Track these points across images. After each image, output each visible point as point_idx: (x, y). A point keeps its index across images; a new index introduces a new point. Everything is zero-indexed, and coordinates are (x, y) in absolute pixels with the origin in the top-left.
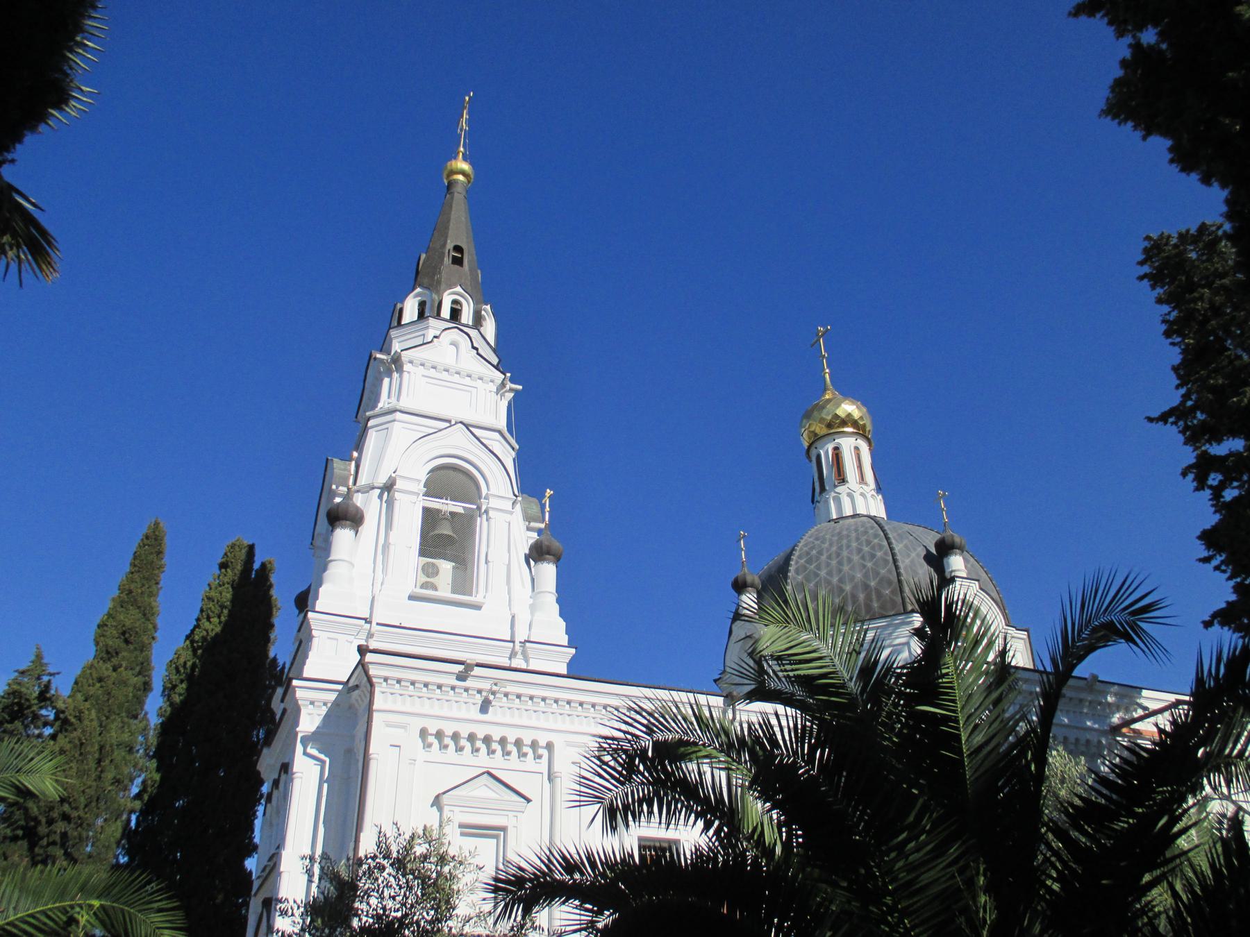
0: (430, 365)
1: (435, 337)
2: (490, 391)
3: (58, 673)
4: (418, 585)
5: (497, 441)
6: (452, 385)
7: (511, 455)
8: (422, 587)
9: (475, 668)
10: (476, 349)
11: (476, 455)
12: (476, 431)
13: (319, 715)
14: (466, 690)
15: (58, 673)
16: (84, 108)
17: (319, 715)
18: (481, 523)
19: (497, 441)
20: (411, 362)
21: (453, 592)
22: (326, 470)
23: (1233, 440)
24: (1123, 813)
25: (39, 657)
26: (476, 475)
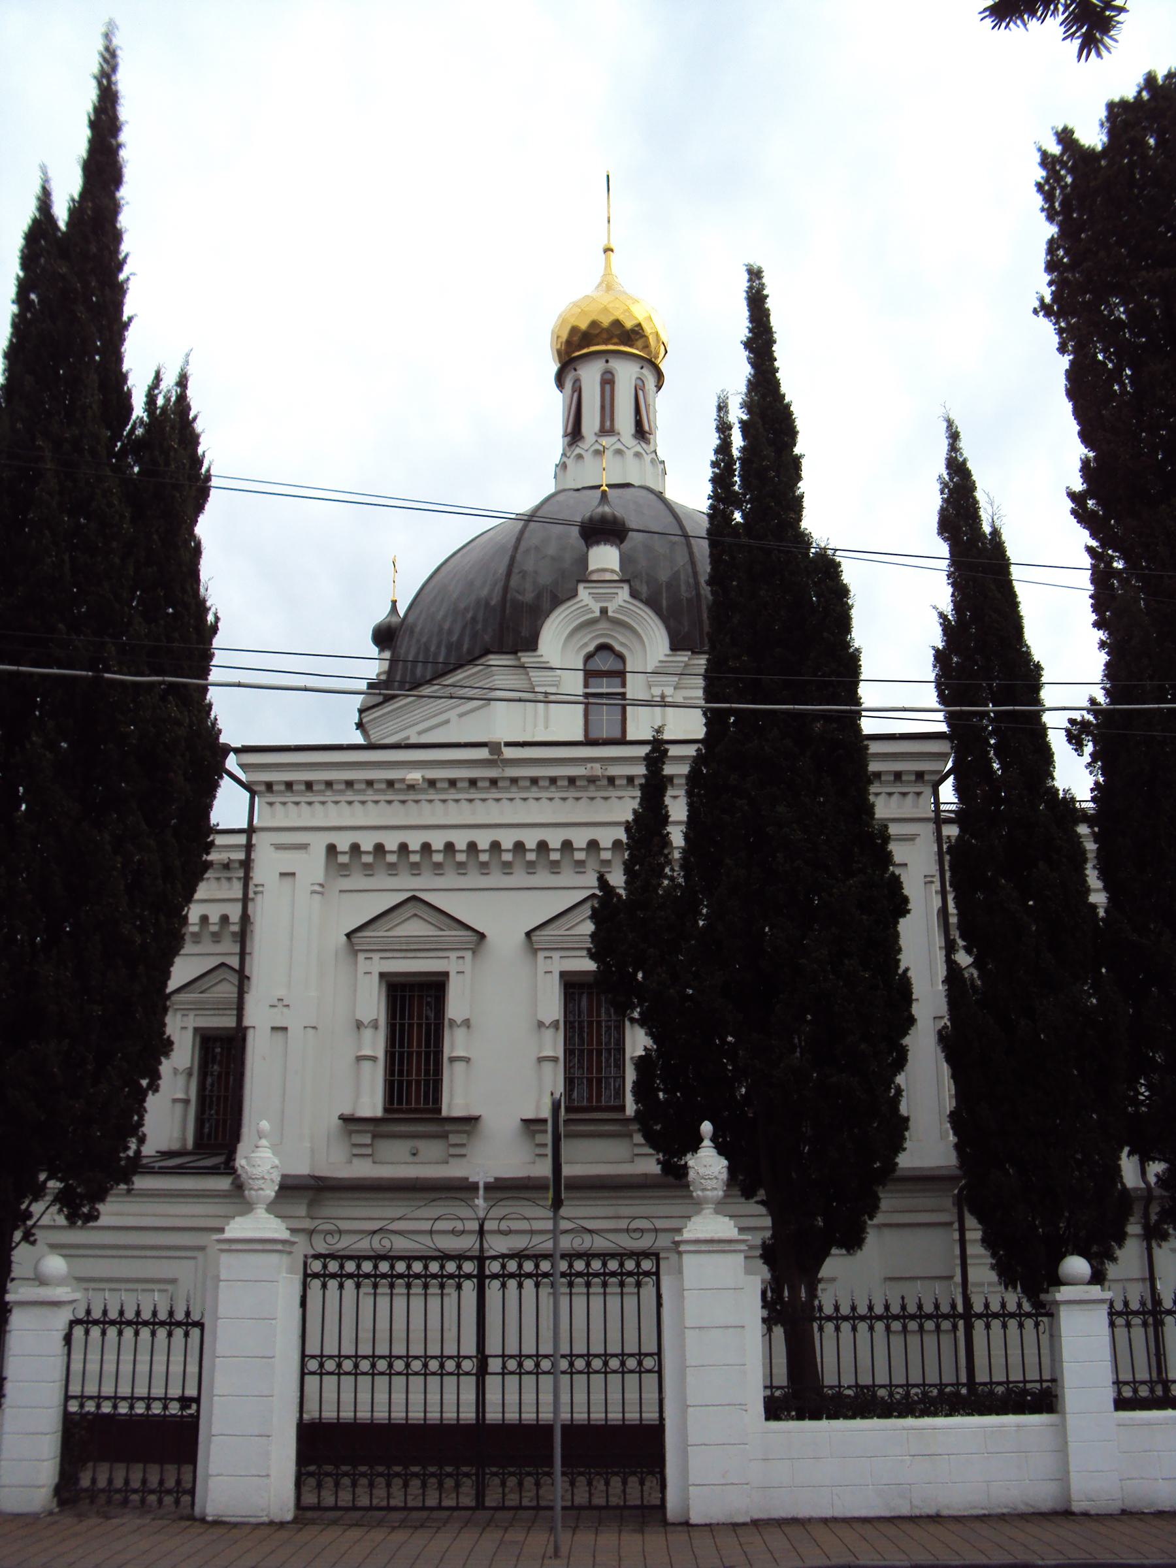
22: (609, 234)
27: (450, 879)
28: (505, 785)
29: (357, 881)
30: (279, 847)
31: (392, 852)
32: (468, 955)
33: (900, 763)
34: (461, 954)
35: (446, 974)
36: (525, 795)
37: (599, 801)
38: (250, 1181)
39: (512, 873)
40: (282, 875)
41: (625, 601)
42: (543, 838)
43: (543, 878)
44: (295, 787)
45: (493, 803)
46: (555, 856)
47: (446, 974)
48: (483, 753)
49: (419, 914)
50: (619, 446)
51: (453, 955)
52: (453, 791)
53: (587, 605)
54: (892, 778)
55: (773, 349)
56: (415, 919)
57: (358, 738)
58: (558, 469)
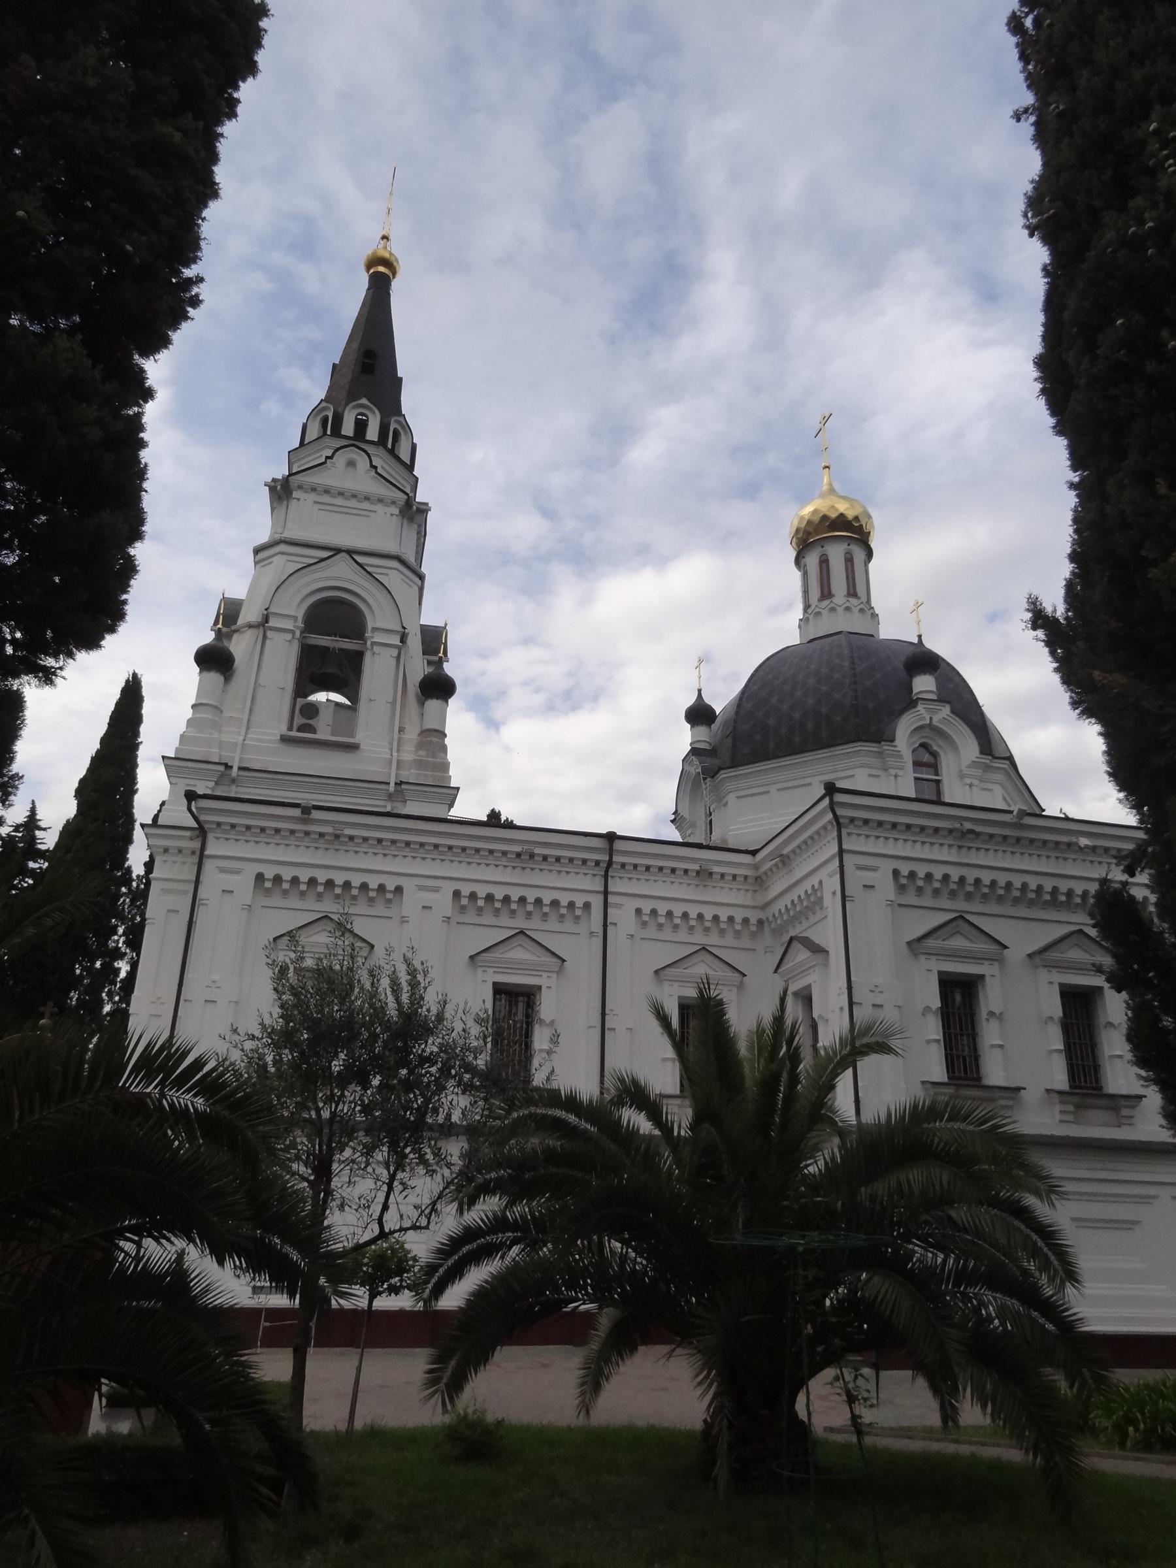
0: (337, 492)
1: (327, 458)
2: (392, 515)
3: (49, 828)
4: (295, 727)
5: (394, 569)
6: (346, 510)
7: (415, 583)
8: (299, 730)
9: (313, 811)
10: (375, 468)
11: (360, 586)
12: (356, 557)
13: (833, 839)
14: (307, 833)
15: (49, 828)
16: (850, 534)
17: (833, 839)
18: (368, 659)
19: (394, 569)
20: (300, 487)
21: (332, 735)
23: (1072, 486)
24: (178, 1142)
25: (33, 811)
26: (355, 601)
27: (553, 924)
28: (286, 834)
29: (276, 900)
30: (223, 870)
31: (373, 890)
32: (555, 975)
33: (423, 837)
34: (730, 988)
35: (539, 988)
36: (577, 870)
37: (222, 840)
38: (1111, 947)
39: (373, 906)
40: (424, 907)
41: (977, 757)
42: (685, 910)
43: (488, 919)
44: (627, 867)
45: (618, 879)
46: (372, 894)
47: (539, 988)
48: (296, 812)
49: (524, 945)
50: (832, 605)
51: (545, 975)
52: (557, 864)
53: (899, 751)
54: (514, 856)
55: (143, 421)
56: (702, 963)
57: (676, 836)
58: (802, 623)
